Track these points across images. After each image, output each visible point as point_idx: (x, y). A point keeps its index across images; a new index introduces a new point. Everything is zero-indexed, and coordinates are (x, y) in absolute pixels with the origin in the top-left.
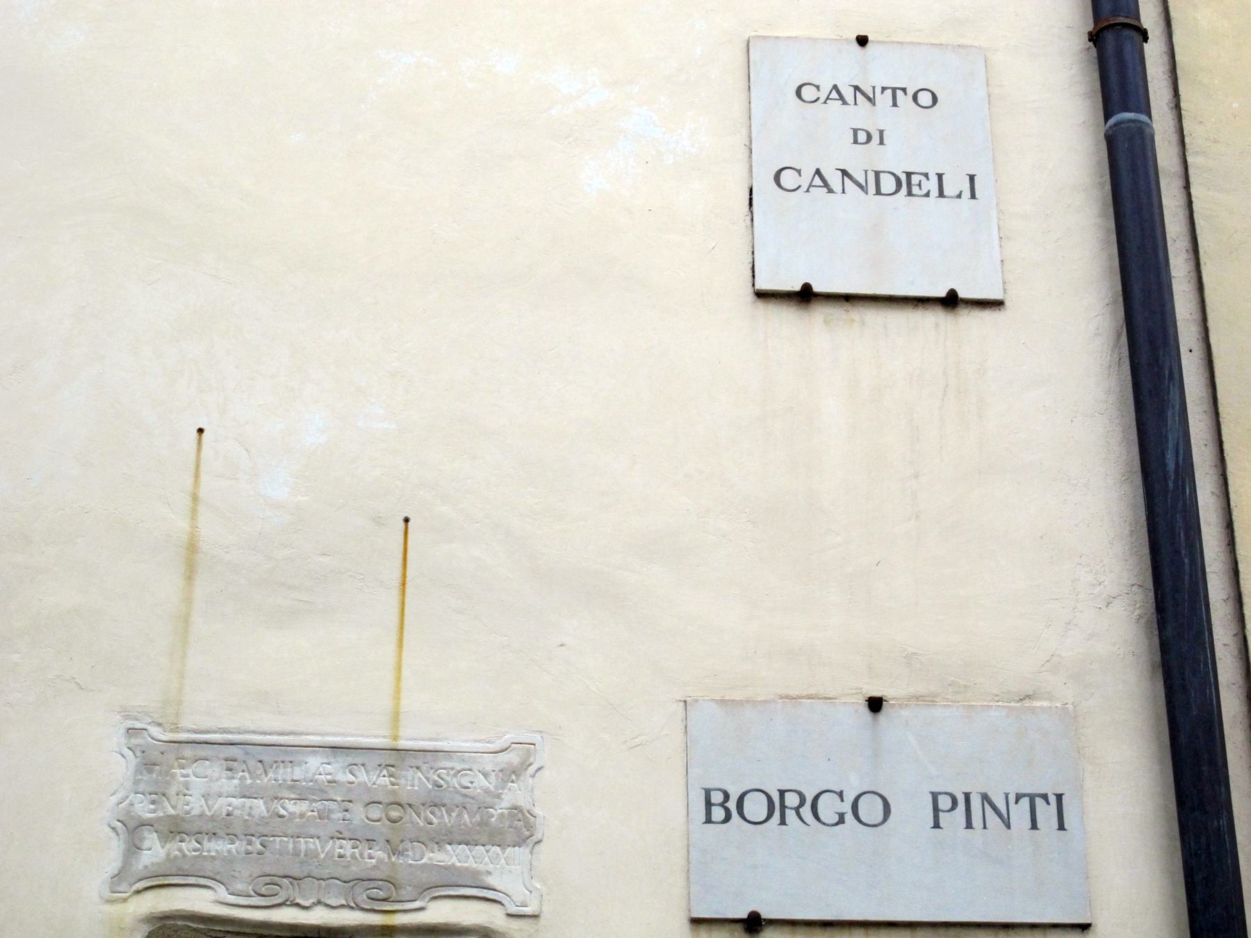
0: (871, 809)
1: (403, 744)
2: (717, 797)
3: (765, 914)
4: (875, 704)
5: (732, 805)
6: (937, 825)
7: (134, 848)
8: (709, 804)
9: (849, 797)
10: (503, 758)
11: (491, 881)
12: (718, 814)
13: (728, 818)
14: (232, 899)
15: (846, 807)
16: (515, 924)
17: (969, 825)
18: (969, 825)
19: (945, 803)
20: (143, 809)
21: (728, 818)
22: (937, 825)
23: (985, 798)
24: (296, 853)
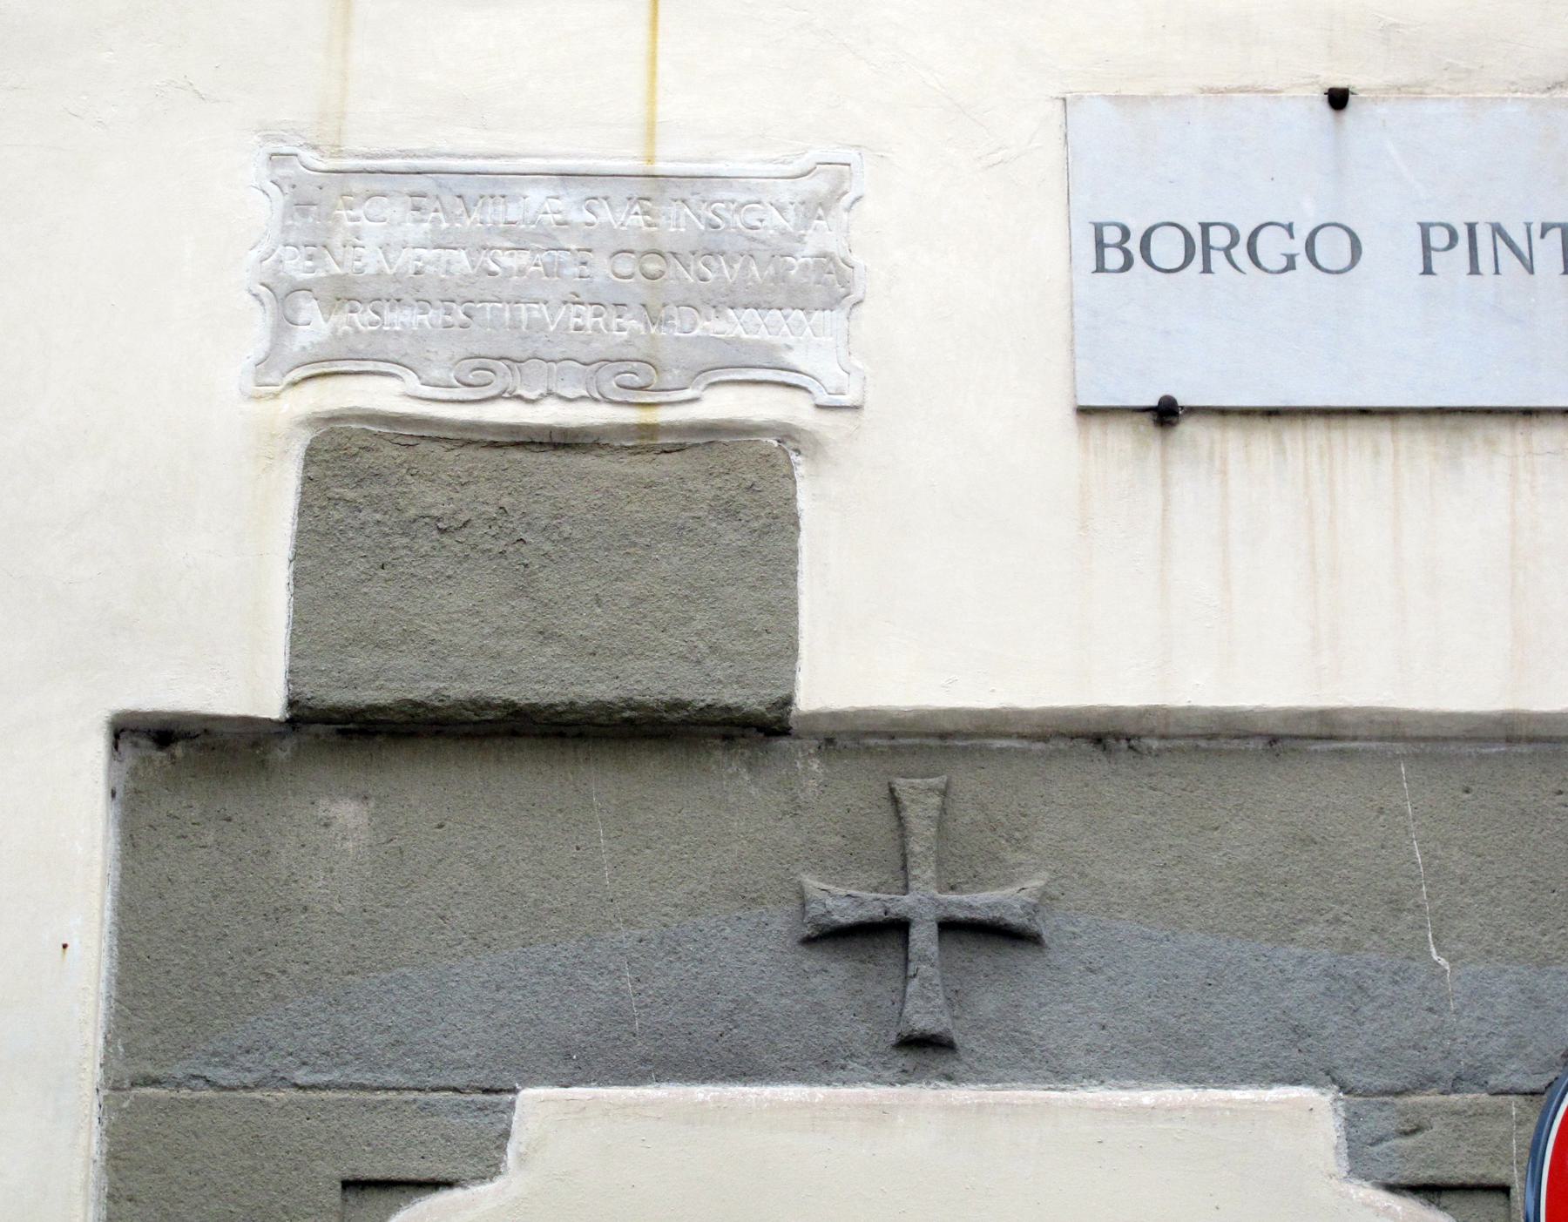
0: (1333, 249)
1: (661, 167)
2: (1112, 235)
3: (1183, 400)
4: (1338, 99)
5: (1134, 246)
6: (1428, 270)
7: (286, 322)
8: (1100, 245)
9: (1302, 234)
10: (805, 184)
11: (792, 359)
12: (1114, 258)
13: (1128, 265)
14: (428, 391)
15: (1298, 246)
16: (828, 419)
17: (1474, 269)
18: (1474, 269)
19: (1439, 238)
20: (297, 267)
21: (1128, 265)
22: (1428, 270)
23: (1498, 230)
24: (515, 326)
